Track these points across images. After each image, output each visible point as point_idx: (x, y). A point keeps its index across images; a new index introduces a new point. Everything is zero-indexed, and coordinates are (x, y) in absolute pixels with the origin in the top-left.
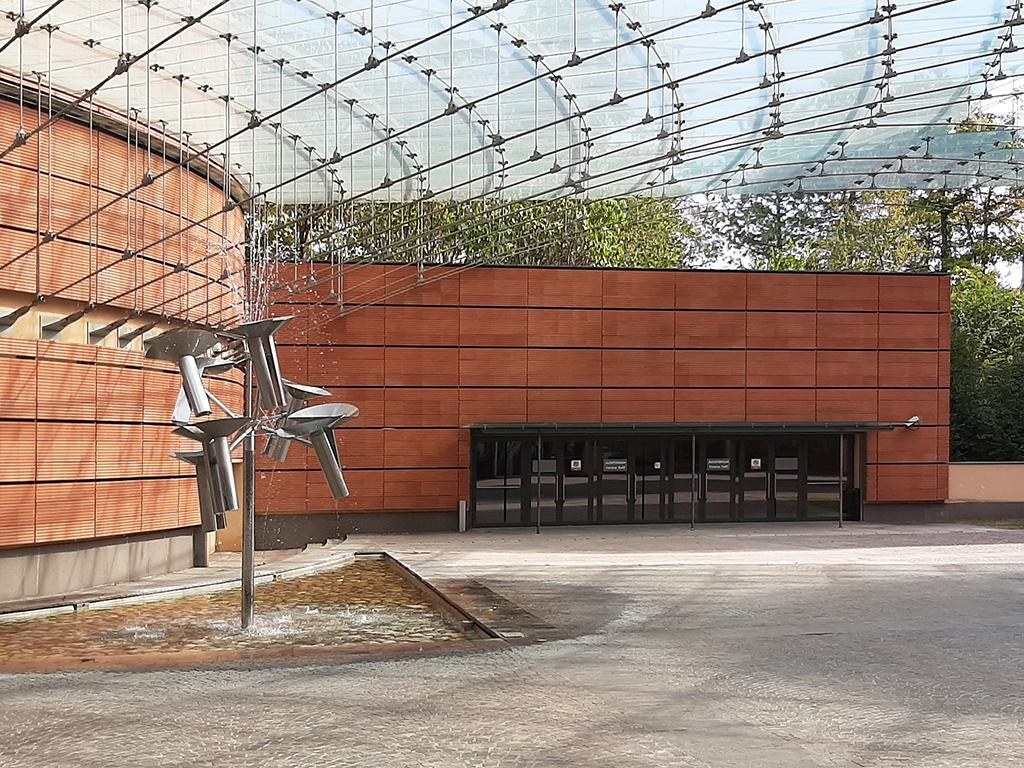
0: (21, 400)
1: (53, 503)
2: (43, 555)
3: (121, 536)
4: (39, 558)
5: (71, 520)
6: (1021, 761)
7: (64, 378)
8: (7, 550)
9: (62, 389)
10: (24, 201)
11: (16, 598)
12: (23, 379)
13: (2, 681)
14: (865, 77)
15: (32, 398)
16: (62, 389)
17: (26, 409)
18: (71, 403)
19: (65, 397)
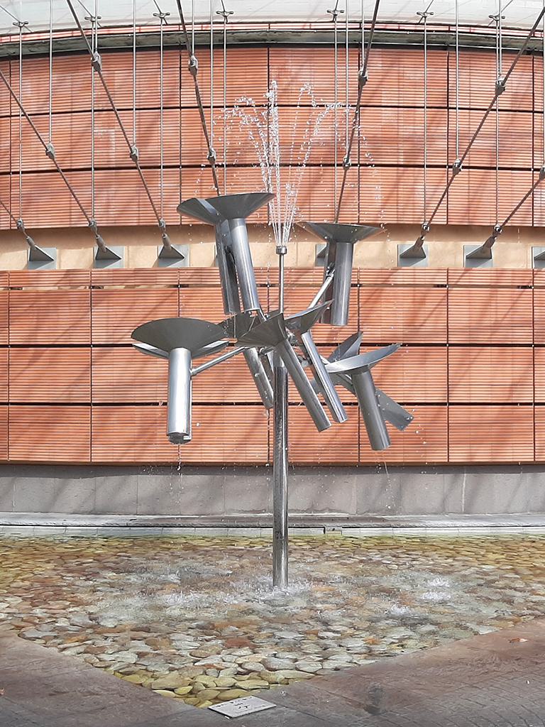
0: (429, 326)
1: (469, 425)
2: (471, 475)
3: (175, 465)
4: (465, 478)
5: (501, 440)
6: (1, 634)
7: (487, 304)
8: (328, 466)
9: (483, 314)
10: (431, 139)
11: (253, 511)
12: (429, 306)
13: (543, 595)
14: (24, 269)
15: (442, 325)
16: (483, 314)
17: (435, 333)
18: (496, 327)
19: (488, 321)
